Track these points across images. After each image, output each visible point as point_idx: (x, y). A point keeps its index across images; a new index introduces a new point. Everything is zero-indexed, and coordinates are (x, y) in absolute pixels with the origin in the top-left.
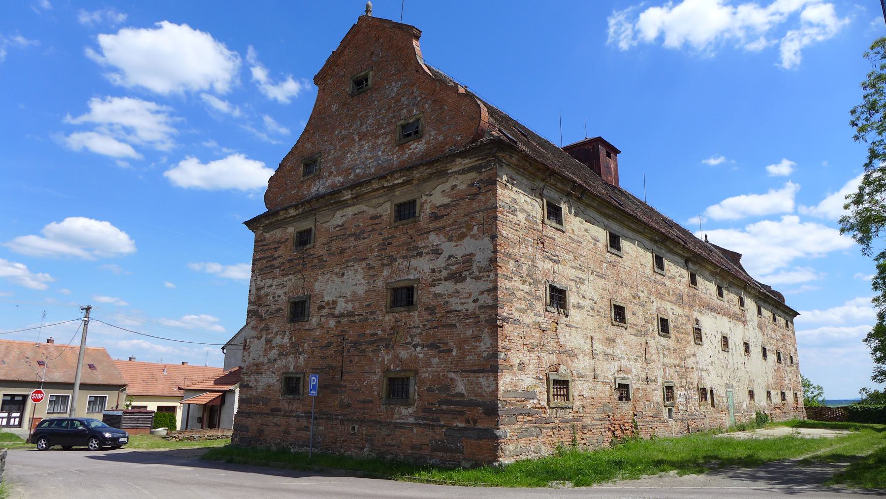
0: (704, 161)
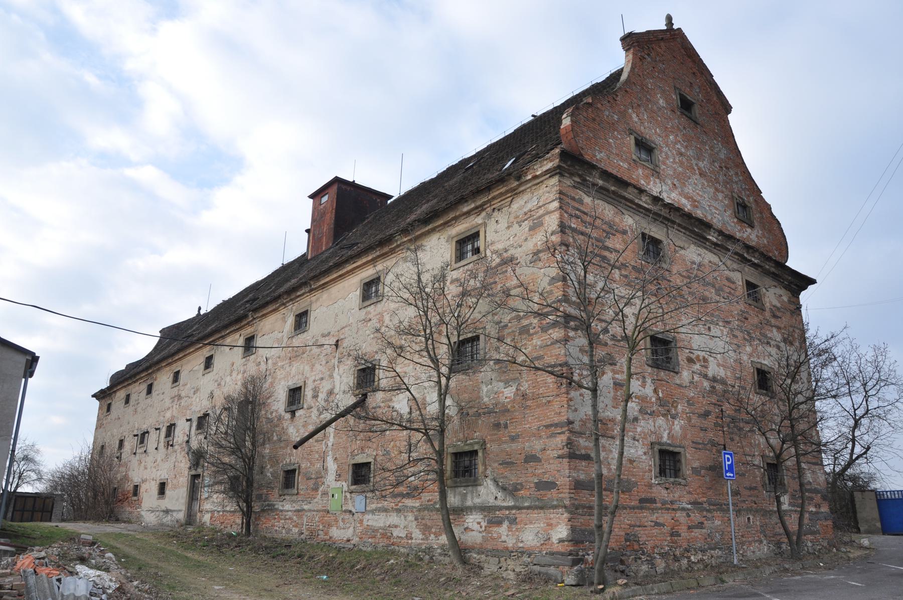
0: (562, 127)
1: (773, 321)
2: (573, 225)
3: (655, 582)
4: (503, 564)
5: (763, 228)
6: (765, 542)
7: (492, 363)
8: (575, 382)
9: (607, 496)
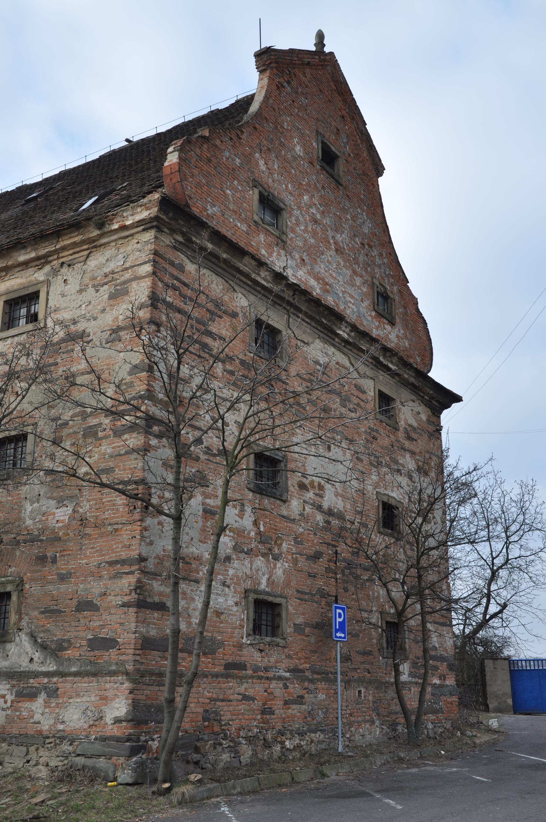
0: (166, 164)
1: (407, 444)
2: (168, 299)
3: (238, 777)
4: (33, 756)
5: (406, 326)
6: (377, 723)
7: (42, 473)
8: (153, 507)
9: (184, 659)
